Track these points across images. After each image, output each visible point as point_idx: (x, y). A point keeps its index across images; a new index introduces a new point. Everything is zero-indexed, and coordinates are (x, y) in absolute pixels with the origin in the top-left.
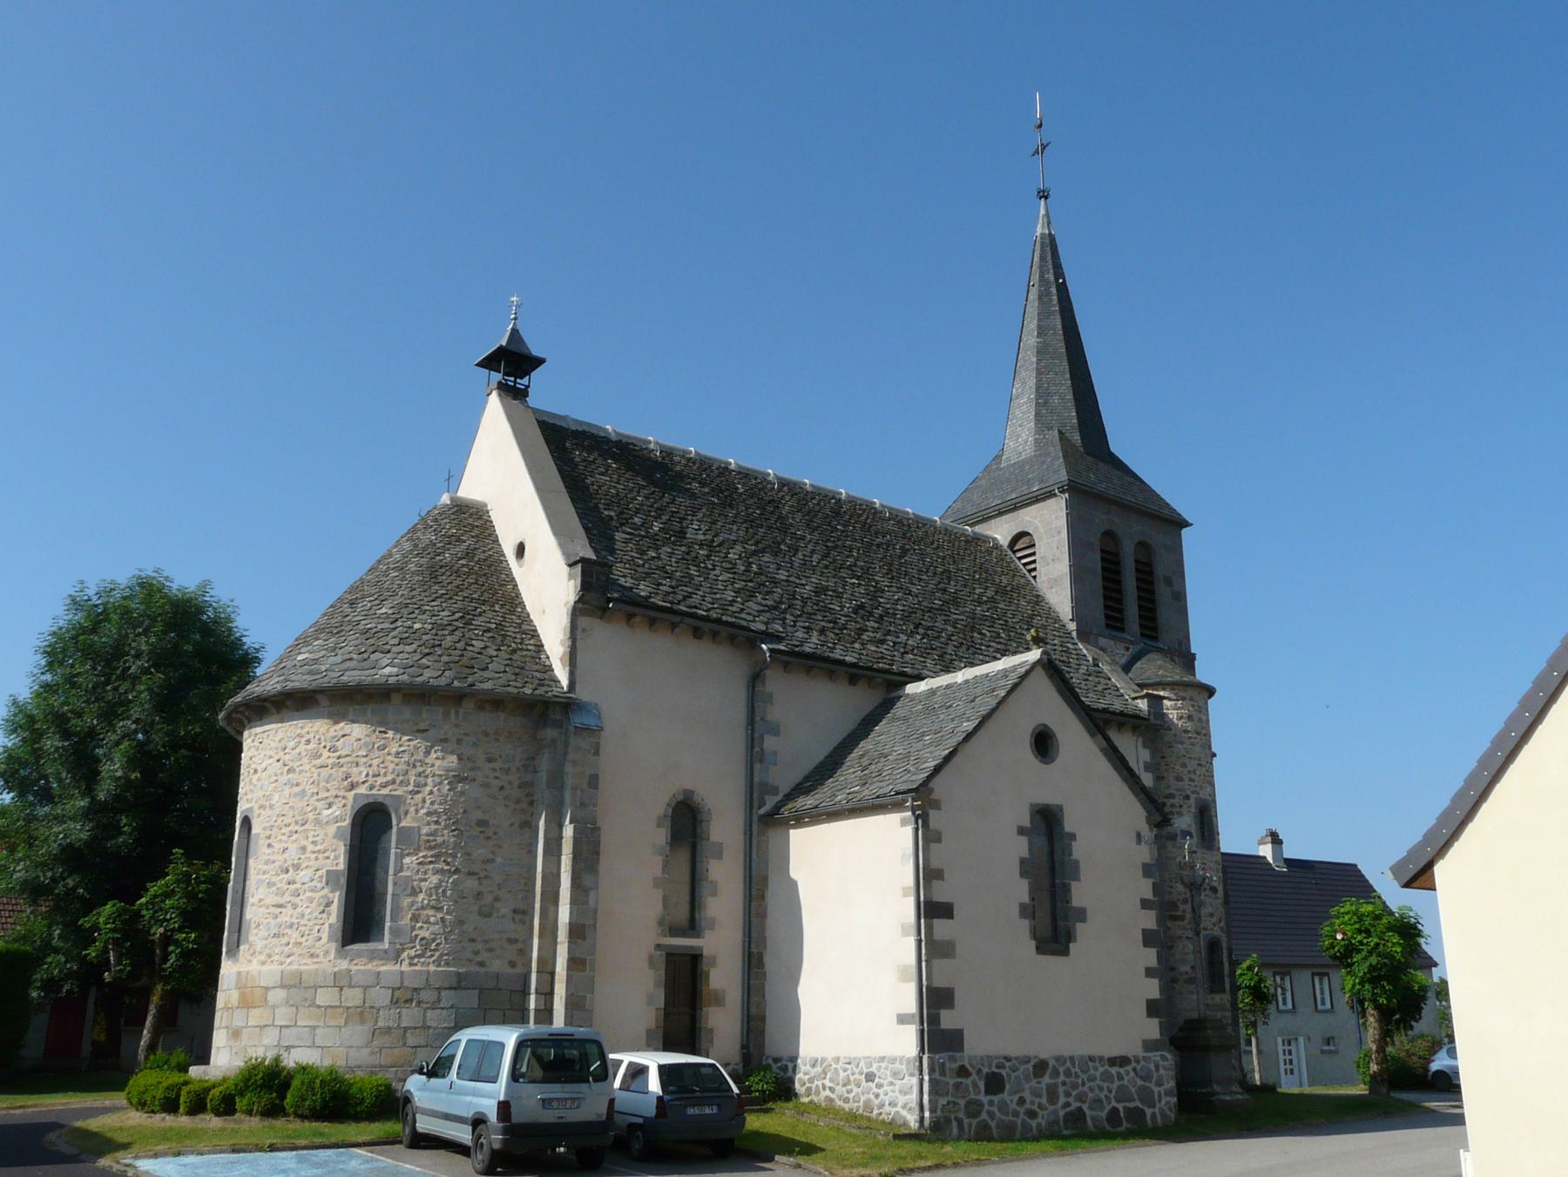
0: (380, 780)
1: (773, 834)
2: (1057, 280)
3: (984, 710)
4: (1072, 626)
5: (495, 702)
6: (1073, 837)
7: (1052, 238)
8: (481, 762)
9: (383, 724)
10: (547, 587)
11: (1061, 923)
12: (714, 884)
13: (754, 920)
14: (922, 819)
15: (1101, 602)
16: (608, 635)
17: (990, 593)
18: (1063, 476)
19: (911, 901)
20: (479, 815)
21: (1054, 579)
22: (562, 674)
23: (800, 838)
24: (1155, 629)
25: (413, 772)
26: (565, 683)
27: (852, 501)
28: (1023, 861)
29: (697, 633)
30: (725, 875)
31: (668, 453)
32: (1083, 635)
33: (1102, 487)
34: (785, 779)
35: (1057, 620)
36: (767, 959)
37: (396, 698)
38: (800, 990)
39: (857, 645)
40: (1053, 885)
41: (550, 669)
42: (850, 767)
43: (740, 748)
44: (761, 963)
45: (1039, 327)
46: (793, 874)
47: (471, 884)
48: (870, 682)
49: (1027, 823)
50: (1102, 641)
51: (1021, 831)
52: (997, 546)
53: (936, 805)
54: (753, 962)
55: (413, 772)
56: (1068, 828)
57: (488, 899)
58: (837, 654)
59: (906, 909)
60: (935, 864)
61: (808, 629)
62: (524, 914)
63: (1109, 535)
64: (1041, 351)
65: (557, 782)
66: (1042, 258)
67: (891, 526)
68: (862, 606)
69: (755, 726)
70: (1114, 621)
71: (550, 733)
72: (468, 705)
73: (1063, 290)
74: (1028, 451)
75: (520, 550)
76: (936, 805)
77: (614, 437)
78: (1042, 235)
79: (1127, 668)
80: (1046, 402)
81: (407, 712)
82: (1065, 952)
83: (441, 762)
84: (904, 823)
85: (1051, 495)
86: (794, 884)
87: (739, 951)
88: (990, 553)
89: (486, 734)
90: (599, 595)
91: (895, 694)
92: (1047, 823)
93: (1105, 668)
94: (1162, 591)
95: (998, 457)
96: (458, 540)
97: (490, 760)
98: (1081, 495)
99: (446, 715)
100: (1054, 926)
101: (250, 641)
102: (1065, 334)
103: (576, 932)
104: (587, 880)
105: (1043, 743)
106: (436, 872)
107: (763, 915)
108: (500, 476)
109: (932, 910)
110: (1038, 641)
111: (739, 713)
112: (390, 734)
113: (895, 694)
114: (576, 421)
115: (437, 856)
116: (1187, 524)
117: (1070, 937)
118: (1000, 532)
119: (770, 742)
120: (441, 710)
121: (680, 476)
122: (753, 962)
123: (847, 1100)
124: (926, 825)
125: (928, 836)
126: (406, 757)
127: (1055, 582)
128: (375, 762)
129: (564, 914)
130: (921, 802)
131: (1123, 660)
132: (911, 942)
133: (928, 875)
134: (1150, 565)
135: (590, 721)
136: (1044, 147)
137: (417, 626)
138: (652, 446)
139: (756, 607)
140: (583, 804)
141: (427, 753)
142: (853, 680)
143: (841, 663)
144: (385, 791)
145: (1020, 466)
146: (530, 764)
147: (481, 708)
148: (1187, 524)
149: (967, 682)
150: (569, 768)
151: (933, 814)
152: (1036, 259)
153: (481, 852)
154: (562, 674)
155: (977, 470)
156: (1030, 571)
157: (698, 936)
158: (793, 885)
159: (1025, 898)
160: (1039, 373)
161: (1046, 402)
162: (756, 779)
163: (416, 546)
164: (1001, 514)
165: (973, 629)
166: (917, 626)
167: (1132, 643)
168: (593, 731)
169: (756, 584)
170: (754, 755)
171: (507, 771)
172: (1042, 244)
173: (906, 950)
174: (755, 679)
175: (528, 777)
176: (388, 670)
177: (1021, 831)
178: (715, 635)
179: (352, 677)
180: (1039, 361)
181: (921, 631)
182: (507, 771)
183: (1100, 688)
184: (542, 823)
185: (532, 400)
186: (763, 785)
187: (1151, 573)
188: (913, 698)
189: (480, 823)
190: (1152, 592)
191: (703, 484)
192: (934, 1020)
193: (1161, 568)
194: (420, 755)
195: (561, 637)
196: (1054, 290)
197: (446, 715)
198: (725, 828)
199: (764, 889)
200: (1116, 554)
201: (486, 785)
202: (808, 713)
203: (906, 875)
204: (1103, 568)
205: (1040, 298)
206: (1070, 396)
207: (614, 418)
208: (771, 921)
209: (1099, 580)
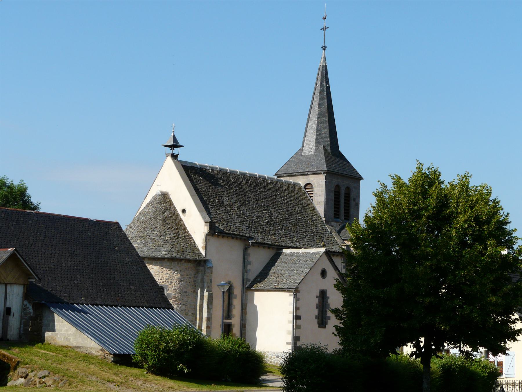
0: (162, 281)
1: (249, 293)
2: (326, 85)
3: (311, 266)
4: (324, 219)
5: (189, 261)
6: (329, 298)
7: (326, 66)
8: (185, 276)
9: (162, 266)
10: (196, 225)
11: (324, 320)
12: (234, 306)
13: (244, 315)
14: (295, 295)
15: (333, 209)
16: (213, 240)
17: (300, 209)
18: (324, 167)
19: (292, 315)
20: (185, 290)
21: (319, 201)
22: (203, 252)
23: (257, 294)
24: (348, 216)
25: (170, 279)
26: (204, 254)
27: (260, 177)
28: (317, 305)
29: (233, 238)
30: (237, 303)
31: (213, 169)
32: (327, 222)
33: (336, 170)
34: (252, 277)
35: (319, 216)
36: (246, 326)
37: (166, 260)
38: (257, 333)
39: (270, 237)
40: (323, 310)
41: (198, 250)
42: (272, 276)
43: (241, 268)
44: (245, 327)
45: (319, 104)
46: (255, 303)
47: (184, 307)
48: (273, 248)
49: (318, 295)
50: (333, 223)
51: (317, 297)
52: (301, 187)
53: (299, 291)
54: (243, 326)
55: (170, 279)
56: (328, 296)
57: (187, 311)
58: (266, 242)
59: (291, 317)
60: (298, 306)
61: (258, 233)
62: (194, 314)
63: (338, 186)
64: (319, 114)
65: (203, 281)
66: (322, 76)
67: (271, 185)
68: (268, 222)
69: (245, 262)
70: (337, 215)
71: (201, 268)
72: (183, 261)
73: (328, 89)
74: (312, 152)
75: (184, 211)
76: (299, 291)
77: (199, 167)
78: (323, 65)
79: (339, 232)
80: (320, 134)
81: (168, 264)
82: (325, 327)
83: (177, 276)
84: (290, 295)
85: (321, 173)
86: (256, 306)
87: (239, 322)
88: (298, 190)
89: (186, 269)
90: (214, 232)
91: (280, 251)
92: (323, 295)
93: (333, 234)
94: (352, 203)
95: (301, 150)
96: (167, 208)
97: (187, 275)
98: (330, 174)
99: (178, 264)
100: (322, 323)
101: (16, 183)
102: (328, 108)
103: (208, 319)
104: (210, 307)
105: (324, 273)
106: (176, 304)
107: (246, 314)
108: (172, 183)
109: (297, 317)
110: (324, 246)
111: (241, 259)
112: (164, 269)
113: (280, 251)
114: (189, 163)
115: (176, 300)
116: (362, 178)
117: (326, 323)
118: (301, 181)
119: (249, 267)
120: (176, 263)
121: (217, 179)
122: (243, 326)
123: (271, 362)
124: (296, 297)
125: (297, 299)
126: (168, 275)
127: (319, 203)
128: (161, 276)
129: (205, 315)
130: (296, 291)
131: (338, 229)
132: (291, 325)
133: (296, 309)
134: (349, 194)
135: (210, 265)
136: (326, 28)
137: (167, 238)
138: (208, 168)
139: (246, 228)
140: (209, 287)
141: (173, 274)
142: (269, 248)
143: (268, 244)
144: (163, 284)
145: (309, 157)
146: (195, 277)
147: (185, 262)
148: (362, 178)
149: (303, 253)
150: (205, 277)
151: (298, 294)
152: (320, 75)
153: (185, 299)
154: (203, 252)
155: (293, 154)
156: (310, 197)
157: (231, 319)
158: (255, 307)
159: (317, 314)
160: (318, 122)
161: (320, 134)
162: (245, 277)
163: (156, 210)
164: (302, 175)
165: (297, 224)
166: (283, 226)
167: (341, 223)
168: (211, 268)
169: (243, 219)
170: (245, 270)
171: (190, 278)
172: (322, 69)
173: (290, 327)
174: (245, 250)
175: (195, 279)
176: (164, 253)
177: (317, 297)
178: (237, 238)
179: (154, 254)
180: (318, 118)
181: (284, 228)
182: (190, 278)
183: (332, 242)
184: (28, 211)
185: (179, 158)
186: (247, 279)
187: (349, 197)
188: (286, 254)
189: (186, 292)
190: (349, 204)
191: (223, 181)
192: (296, 344)
193: (352, 196)
194: (171, 274)
195: (202, 241)
196: (325, 89)
197: (178, 264)
198: (237, 291)
199: (247, 307)
200: (339, 192)
201: (186, 282)
202: (258, 258)
203: (291, 308)
204: (335, 198)
205: (320, 92)
206: (328, 133)
207: (199, 160)
208: (248, 315)
209: (333, 203)
